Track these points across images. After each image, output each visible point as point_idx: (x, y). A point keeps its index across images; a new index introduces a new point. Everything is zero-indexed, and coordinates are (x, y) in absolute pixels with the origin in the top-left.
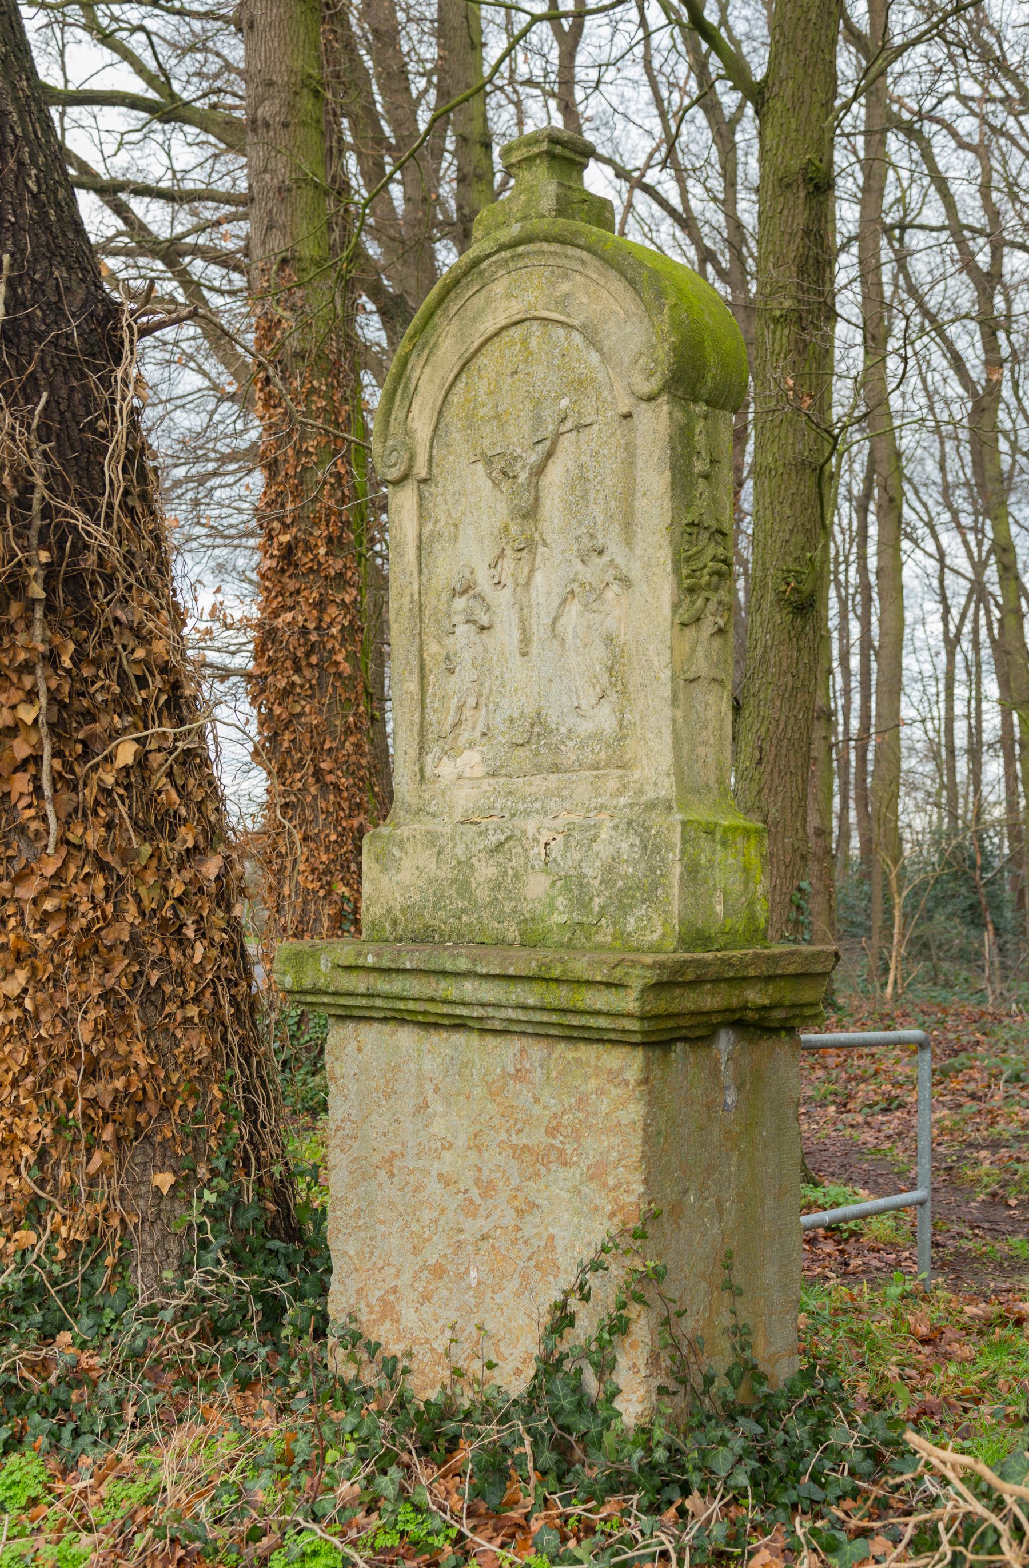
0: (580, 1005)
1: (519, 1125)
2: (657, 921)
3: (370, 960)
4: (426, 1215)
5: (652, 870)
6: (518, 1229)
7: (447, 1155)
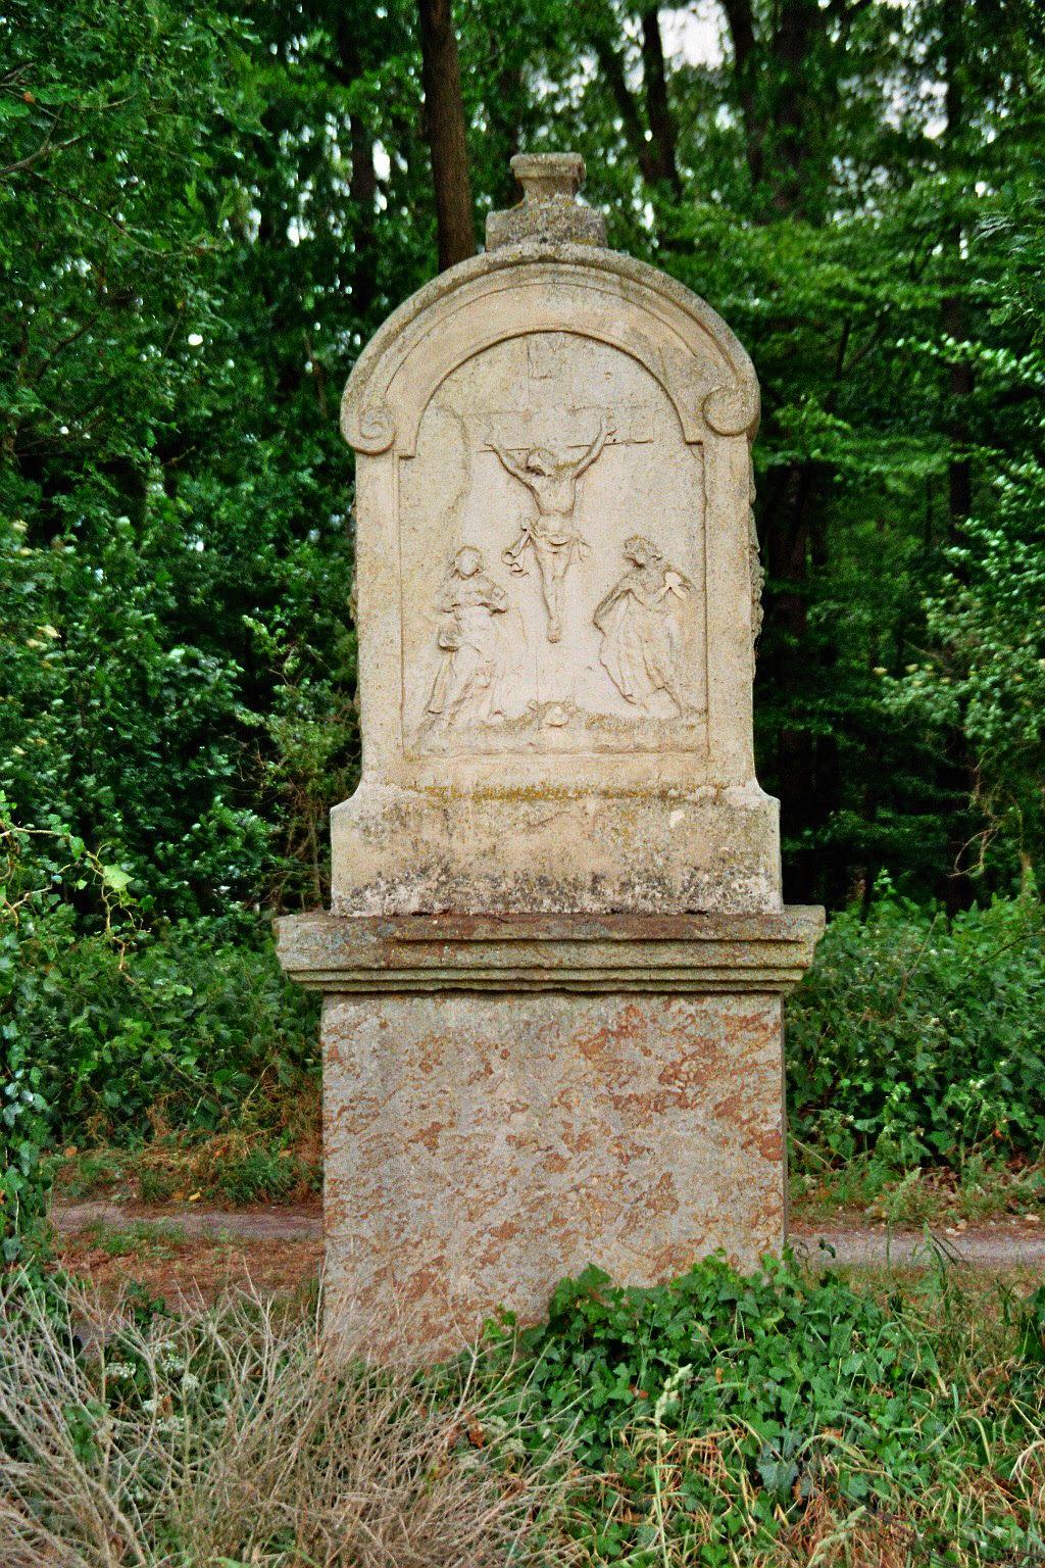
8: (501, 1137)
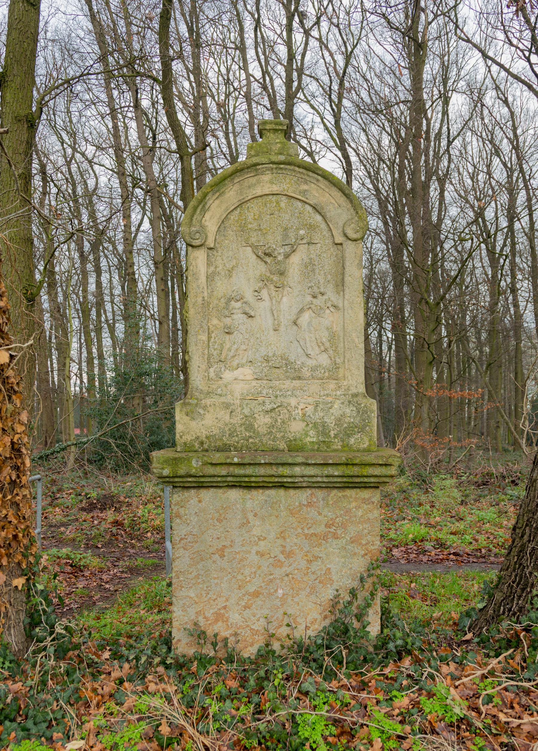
0: (365, 474)
1: (309, 525)
2: (366, 439)
3: (236, 460)
4: (247, 572)
5: (364, 420)
6: (309, 568)
7: (262, 543)
8: (254, 552)
